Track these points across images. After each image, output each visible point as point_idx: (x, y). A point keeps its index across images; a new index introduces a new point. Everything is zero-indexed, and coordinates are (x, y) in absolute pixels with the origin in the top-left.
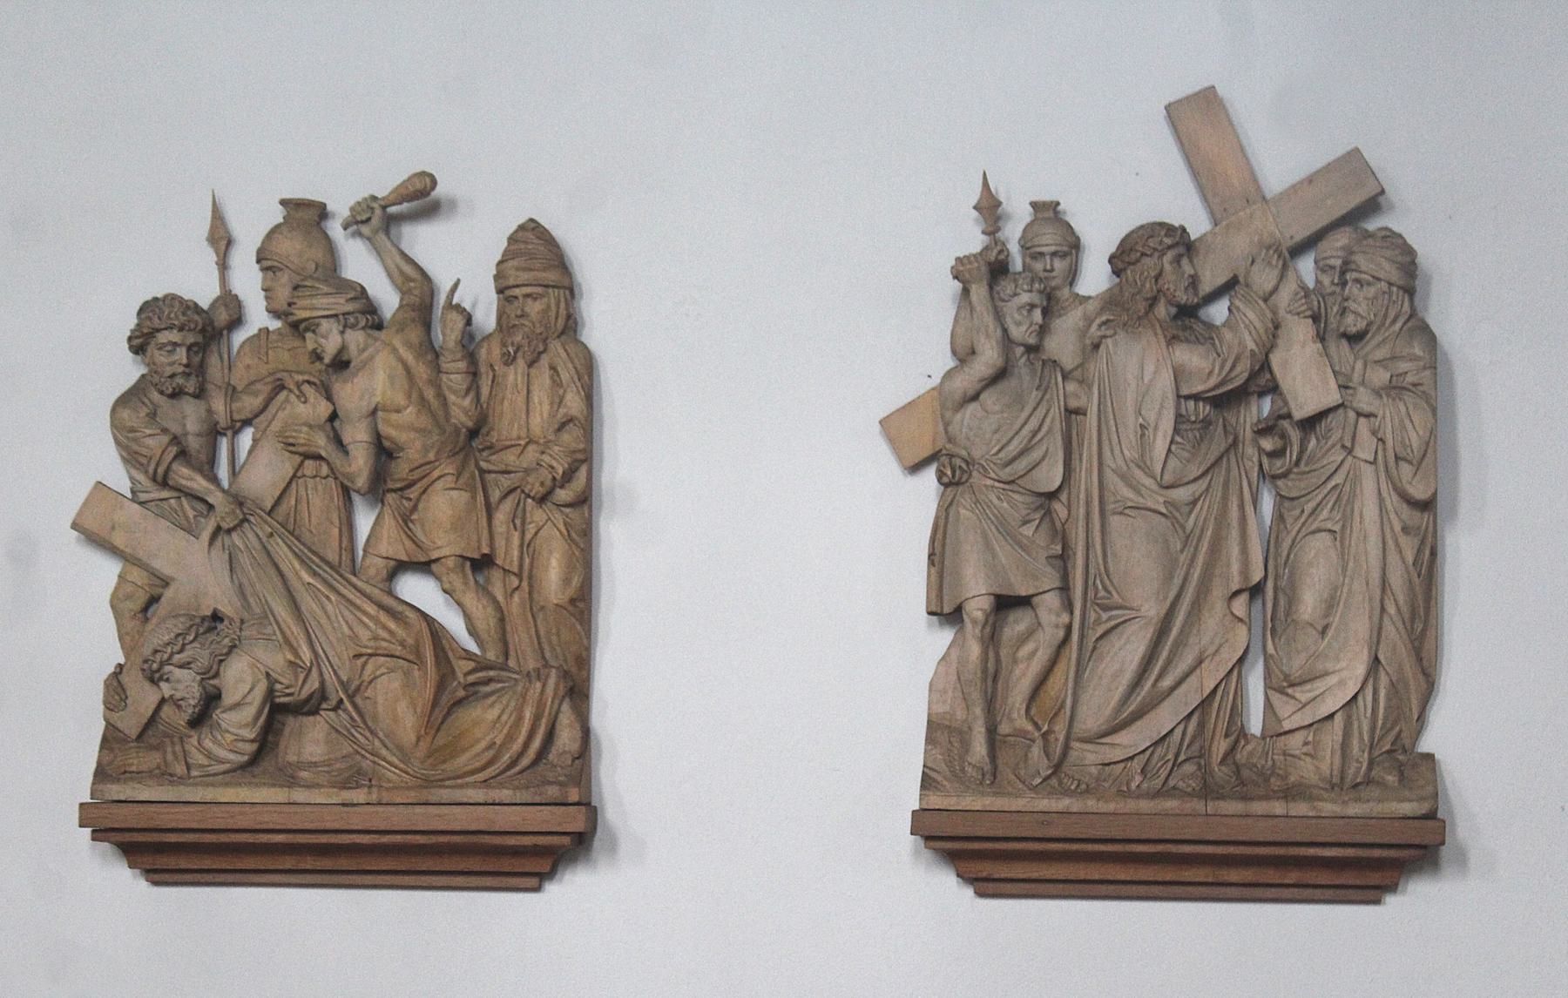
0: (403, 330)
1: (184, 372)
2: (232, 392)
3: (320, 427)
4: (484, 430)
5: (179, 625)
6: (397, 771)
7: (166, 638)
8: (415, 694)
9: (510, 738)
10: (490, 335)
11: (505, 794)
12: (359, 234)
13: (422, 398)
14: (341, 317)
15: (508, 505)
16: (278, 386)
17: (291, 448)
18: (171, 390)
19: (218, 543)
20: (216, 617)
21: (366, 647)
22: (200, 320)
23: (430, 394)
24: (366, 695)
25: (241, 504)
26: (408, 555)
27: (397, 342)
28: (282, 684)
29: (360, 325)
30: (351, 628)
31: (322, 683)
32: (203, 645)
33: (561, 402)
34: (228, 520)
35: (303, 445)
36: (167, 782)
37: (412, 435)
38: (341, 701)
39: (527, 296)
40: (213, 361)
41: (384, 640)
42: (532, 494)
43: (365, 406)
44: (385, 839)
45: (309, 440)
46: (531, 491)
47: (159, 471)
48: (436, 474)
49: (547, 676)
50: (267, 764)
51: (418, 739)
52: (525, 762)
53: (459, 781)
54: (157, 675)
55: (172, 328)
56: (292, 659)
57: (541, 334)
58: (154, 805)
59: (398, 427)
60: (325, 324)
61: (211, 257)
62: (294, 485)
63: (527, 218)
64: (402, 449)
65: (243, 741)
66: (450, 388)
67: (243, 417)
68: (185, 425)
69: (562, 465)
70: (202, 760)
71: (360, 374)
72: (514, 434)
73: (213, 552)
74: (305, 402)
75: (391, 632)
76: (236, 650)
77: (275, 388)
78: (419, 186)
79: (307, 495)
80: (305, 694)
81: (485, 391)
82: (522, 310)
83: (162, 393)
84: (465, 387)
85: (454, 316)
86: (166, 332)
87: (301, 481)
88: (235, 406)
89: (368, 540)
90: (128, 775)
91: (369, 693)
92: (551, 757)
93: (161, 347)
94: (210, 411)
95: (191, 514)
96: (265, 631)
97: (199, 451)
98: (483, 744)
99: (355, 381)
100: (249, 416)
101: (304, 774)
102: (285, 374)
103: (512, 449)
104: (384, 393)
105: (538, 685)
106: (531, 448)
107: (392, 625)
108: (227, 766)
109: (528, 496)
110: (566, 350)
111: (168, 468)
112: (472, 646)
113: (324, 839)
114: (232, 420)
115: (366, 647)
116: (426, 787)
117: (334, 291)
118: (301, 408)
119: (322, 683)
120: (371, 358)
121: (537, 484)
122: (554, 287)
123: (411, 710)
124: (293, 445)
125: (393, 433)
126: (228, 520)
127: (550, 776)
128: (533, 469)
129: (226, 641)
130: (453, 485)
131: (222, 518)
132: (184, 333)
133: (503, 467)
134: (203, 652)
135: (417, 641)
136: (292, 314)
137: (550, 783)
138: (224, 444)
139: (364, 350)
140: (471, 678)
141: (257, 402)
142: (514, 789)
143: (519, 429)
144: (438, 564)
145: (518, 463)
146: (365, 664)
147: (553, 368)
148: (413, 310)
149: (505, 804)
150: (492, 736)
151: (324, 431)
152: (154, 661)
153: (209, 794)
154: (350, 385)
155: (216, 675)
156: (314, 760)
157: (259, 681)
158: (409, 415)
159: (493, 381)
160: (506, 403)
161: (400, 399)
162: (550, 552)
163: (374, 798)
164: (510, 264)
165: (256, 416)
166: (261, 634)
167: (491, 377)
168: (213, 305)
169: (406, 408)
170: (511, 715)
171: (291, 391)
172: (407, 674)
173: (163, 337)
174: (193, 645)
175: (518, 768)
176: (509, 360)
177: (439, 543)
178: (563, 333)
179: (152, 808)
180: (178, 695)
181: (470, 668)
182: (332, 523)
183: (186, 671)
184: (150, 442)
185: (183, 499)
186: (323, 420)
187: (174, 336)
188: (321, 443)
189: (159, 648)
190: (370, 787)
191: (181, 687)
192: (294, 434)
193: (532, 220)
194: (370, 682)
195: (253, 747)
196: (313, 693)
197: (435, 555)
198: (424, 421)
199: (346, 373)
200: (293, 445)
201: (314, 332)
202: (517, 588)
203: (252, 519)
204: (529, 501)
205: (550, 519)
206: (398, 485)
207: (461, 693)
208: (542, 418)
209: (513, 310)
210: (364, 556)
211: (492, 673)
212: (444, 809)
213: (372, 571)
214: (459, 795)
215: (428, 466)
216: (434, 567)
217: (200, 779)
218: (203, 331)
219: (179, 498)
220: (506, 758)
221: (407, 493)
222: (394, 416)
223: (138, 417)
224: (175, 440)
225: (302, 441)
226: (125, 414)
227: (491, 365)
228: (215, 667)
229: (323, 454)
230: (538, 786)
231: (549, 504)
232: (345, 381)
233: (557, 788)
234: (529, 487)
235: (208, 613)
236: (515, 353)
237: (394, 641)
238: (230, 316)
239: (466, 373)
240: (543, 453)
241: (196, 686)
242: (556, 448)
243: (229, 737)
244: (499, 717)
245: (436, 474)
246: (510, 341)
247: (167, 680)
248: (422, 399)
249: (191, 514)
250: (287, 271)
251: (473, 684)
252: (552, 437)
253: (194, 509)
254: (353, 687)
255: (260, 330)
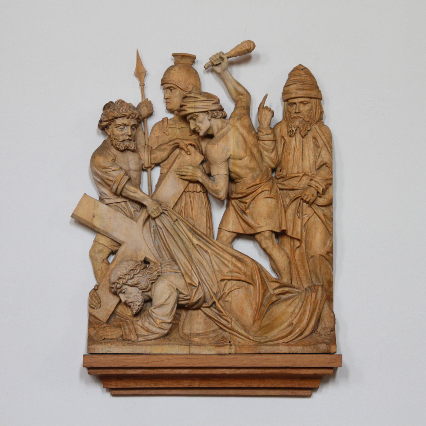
0: (240, 119)
1: (128, 139)
2: (151, 151)
3: (198, 167)
4: (279, 169)
5: (131, 265)
6: (243, 338)
7: (125, 272)
8: (251, 299)
9: (300, 321)
10: (281, 122)
11: (299, 349)
12: (213, 71)
13: (252, 153)
14: (210, 112)
15: (293, 206)
16: (176, 146)
17: (184, 177)
18: (124, 148)
19: (147, 223)
20: (146, 262)
21: (227, 276)
22: (137, 113)
23: (255, 151)
24: (226, 300)
25: (160, 205)
26: (244, 231)
27: (238, 124)
28: (184, 294)
29: (219, 117)
30: (219, 267)
31: (204, 293)
32: (143, 275)
33: (319, 155)
34: (155, 213)
35: (190, 176)
36: (126, 344)
37: (247, 171)
38: (214, 303)
39: (301, 102)
40: (140, 133)
41: (236, 272)
42: (308, 200)
43: (224, 156)
44: (239, 371)
45: (193, 173)
46: (307, 199)
47: (119, 188)
48: (260, 190)
49: (317, 290)
50: (174, 335)
51: (254, 322)
52: (307, 333)
53: (275, 342)
54: (119, 290)
55: (123, 117)
56: (190, 282)
57: (309, 121)
58: (122, 355)
59: (240, 167)
60: (201, 116)
61: (137, 82)
62: (184, 196)
63: (298, 64)
64: (241, 178)
65: (166, 323)
66: (263, 148)
67: (156, 162)
68: (128, 165)
69: (322, 186)
70: (144, 333)
71: (222, 141)
72: (295, 171)
73: (145, 229)
74: (189, 155)
75: (239, 268)
76: (160, 277)
77: (174, 148)
78: (247, 47)
79: (191, 200)
80: (195, 299)
81: (280, 149)
82: (299, 110)
83: (118, 149)
84: (272, 148)
85: (267, 112)
86: (121, 119)
87: (187, 193)
88: (153, 156)
89: (221, 223)
90: (105, 340)
91: (227, 299)
92: (319, 330)
93: (117, 127)
94: (140, 159)
95: (132, 210)
96: (173, 268)
97: (135, 179)
98: (286, 324)
99: (219, 144)
100: (160, 161)
101: (196, 339)
102: (180, 141)
103: (295, 178)
104: (234, 151)
105: (314, 295)
106: (304, 178)
107: (239, 265)
108: (157, 336)
109: (305, 201)
110: (320, 130)
111: (124, 187)
112: (274, 275)
113: (208, 372)
114: (151, 164)
115: (227, 276)
116: (259, 345)
117: (206, 99)
118: (188, 157)
119: (204, 293)
120: (227, 132)
121: (310, 195)
122: (314, 98)
123: (250, 307)
124: (184, 176)
125: (238, 170)
126: (155, 213)
127: (319, 339)
128: (307, 188)
129: (155, 273)
130: (269, 196)
131: (152, 212)
132: (129, 119)
133: (291, 187)
134: (143, 279)
135: (252, 273)
136: (185, 110)
137: (321, 343)
138: (145, 175)
139: (222, 129)
140: (277, 291)
141: (164, 154)
142: (303, 346)
143: (298, 168)
144: (260, 235)
145: (298, 185)
146: (225, 285)
147: (314, 138)
148: (244, 109)
149: (298, 354)
150: (291, 320)
151: (200, 169)
152: (118, 283)
153: (148, 350)
154: (216, 146)
155: (150, 290)
156: (198, 332)
157: (173, 293)
158: (246, 160)
159: (284, 145)
160: (291, 156)
161: (241, 153)
162: (316, 229)
163: (233, 351)
164: (292, 87)
165: (163, 161)
166: (172, 269)
167: (283, 143)
168: (140, 105)
169: (245, 157)
170: (300, 309)
171: (182, 149)
172: (247, 289)
173: (119, 121)
174: (138, 275)
175: (303, 336)
176: (291, 134)
177: (261, 224)
178: (318, 122)
179: (120, 357)
180: (130, 300)
181: (276, 286)
182: (202, 215)
183: (134, 288)
184: (115, 174)
185: (128, 202)
186: (199, 164)
187: (124, 121)
188: (200, 175)
189: (121, 277)
190: (231, 345)
191: (132, 296)
192: (185, 170)
193: (300, 65)
194: (228, 293)
195: (168, 327)
196: (200, 299)
197: (259, 230)
198: (253, 164)
199: (213, 140)
200: (184, 176)
201: (194, 120)
202: (298, 247)
203: (166, 212)
204: (305, 204)
205: (315, 212)
206: (240, 196)
207: (274, 299)
208: (310, 163)
209: (293, 109)
210: (219, 232)
211: (286, 289)
212: (271, 357)
213: (224, 239)
214: (275, 349)
215: (256, 187)
216: (257, 237)
217: (143, 342)
218: (138, 118)
219: (126, 202)
220: (297, 330)
221: (244, 200)
222: (238, 162)
223: (108, 161)
224: (126, 174)
225: (189, 174)
226: (101, 160)
227: (283, 137)
228: (150, 286)
229: (200, 180)
230: (315, 344)
231: (315, 205)
232: (214, 144)
233: (325, 345)
234: (306, 197)
235: (143, 259)
236: (296, 131)
237: (240, 273)
238: (149, 111)
239: (273, 140)
240: (311, 180)
241: (140, 296)
242: (319, 178)
243: (158, 322)
244: (294, 310)
245: (260, 190)
246: (292, 125)
247: (124, 293)
248: (252, 154)
249: (132, 210)
250: (178, 89)
251: (279, 294)
252: (315, 173)
253: (134, 208)
254: (219, 296)
255: (163, 119)
